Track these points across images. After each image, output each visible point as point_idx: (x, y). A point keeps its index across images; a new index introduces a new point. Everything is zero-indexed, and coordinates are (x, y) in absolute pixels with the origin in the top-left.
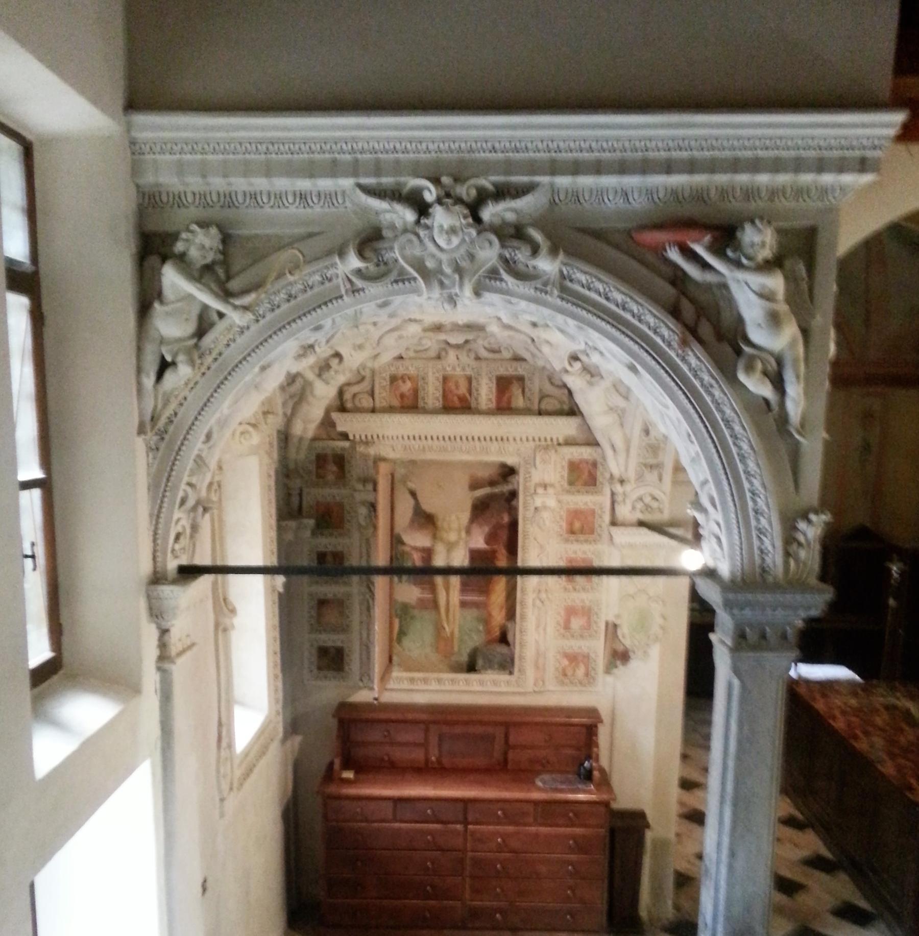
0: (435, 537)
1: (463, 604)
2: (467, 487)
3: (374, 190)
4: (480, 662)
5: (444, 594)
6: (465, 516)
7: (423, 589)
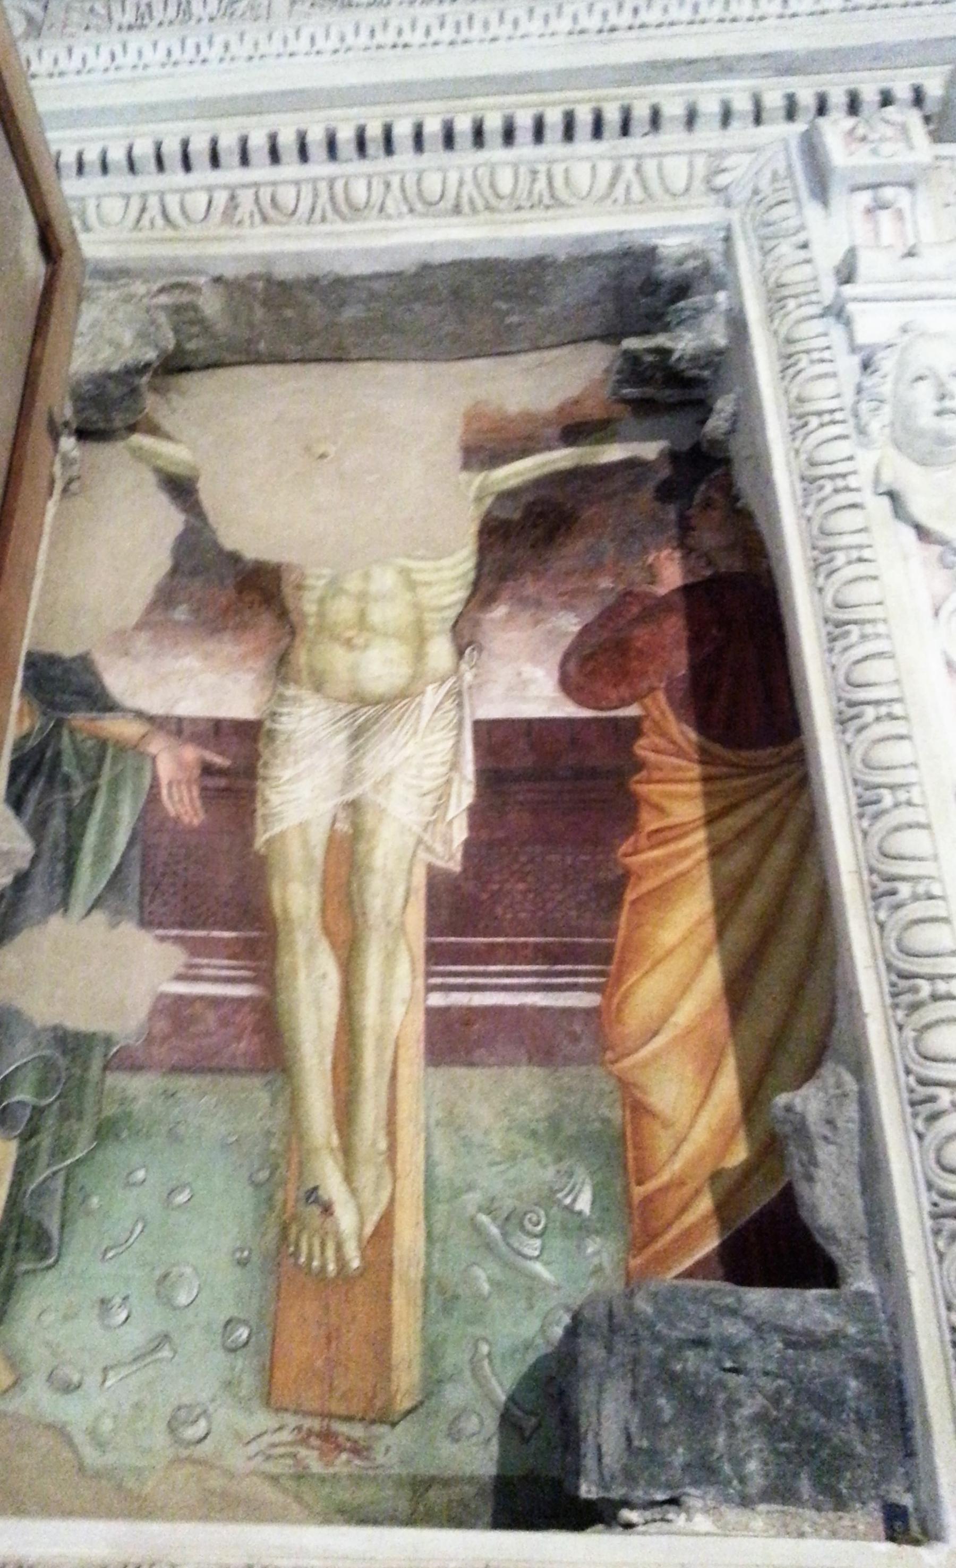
0: (281, 668)
1: (452, 1039)
2: (452, 452)
3: (395, 1123)
4: (608, 1419)
5: (327, 965)
6: (450, 571)
7: (195, 948)
